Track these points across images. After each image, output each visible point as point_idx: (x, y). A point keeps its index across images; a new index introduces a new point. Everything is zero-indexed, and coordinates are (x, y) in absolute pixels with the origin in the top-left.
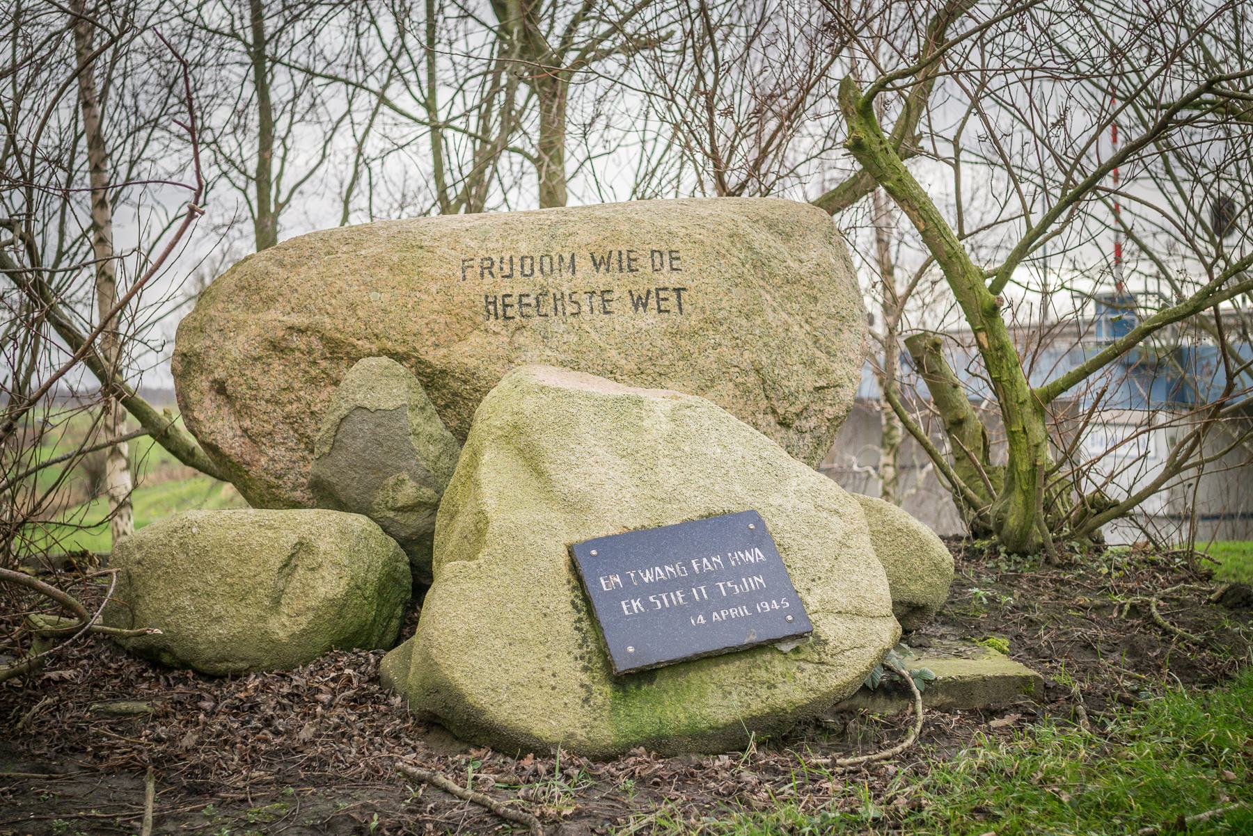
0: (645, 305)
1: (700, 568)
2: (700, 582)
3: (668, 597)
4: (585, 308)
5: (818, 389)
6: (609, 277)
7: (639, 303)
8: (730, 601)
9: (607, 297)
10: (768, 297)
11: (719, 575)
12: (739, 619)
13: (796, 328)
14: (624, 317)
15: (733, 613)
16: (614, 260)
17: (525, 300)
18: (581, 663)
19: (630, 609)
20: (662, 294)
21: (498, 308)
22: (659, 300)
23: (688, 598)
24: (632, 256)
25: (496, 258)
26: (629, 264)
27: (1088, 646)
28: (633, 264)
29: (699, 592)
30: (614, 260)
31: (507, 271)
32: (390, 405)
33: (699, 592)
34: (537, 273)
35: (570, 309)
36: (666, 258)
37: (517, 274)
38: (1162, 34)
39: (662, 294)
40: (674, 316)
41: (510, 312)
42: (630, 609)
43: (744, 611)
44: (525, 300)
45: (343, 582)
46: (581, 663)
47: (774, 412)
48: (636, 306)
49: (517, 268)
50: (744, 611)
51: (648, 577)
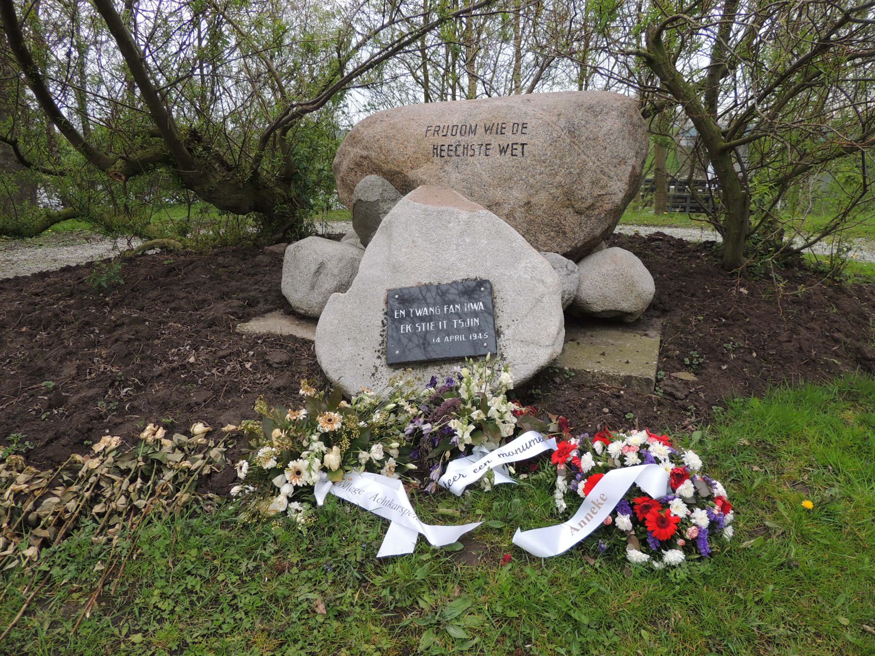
0: (505, 152)
1: (448, 310)
2: (444, 319)
3: (426, 325)
4: (477, 153)
5: (599, 196)
6: (490, 137)
7: (503, 151)
8: (459, 331)
9: (488, 147)
10: (576, 147)
11: (458, 315)
12: (459, 342)
13: (591, 164)
14: (496, 157)
15: (456, 338)
16: (495, 128)
17: (451, 148)
18: (377, 354)
19: (404, 330)
20: (515, 147)
21: (438, 151)
22: (513, 149)
23: (436, 326)
24: (504, 126)
25: (442, 127)
26: (501, 130)
27: (355, 554)
28: (503, 131)
29: (443, 324)
30: (495, 128)
31: (445, 133)
32: (373, 199)
33: (443, 324)
34: (458, 133)
35: (470, 153)
36: (520, 127)
37: (449, 134)
38: (426, 77)
39: (515, 147)
40: (519, 158)
41: (443, 154)
42: (404, 330)
43: (462, 338)
44: (451, 148)
45: (335, 283)
46: (377, 354)
47: (573, 207)
48: (501, 152)
49: (450, 131)
50: (462, 338)
51: (419, 313)
